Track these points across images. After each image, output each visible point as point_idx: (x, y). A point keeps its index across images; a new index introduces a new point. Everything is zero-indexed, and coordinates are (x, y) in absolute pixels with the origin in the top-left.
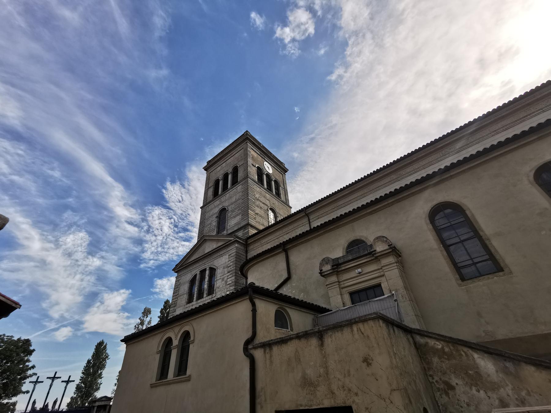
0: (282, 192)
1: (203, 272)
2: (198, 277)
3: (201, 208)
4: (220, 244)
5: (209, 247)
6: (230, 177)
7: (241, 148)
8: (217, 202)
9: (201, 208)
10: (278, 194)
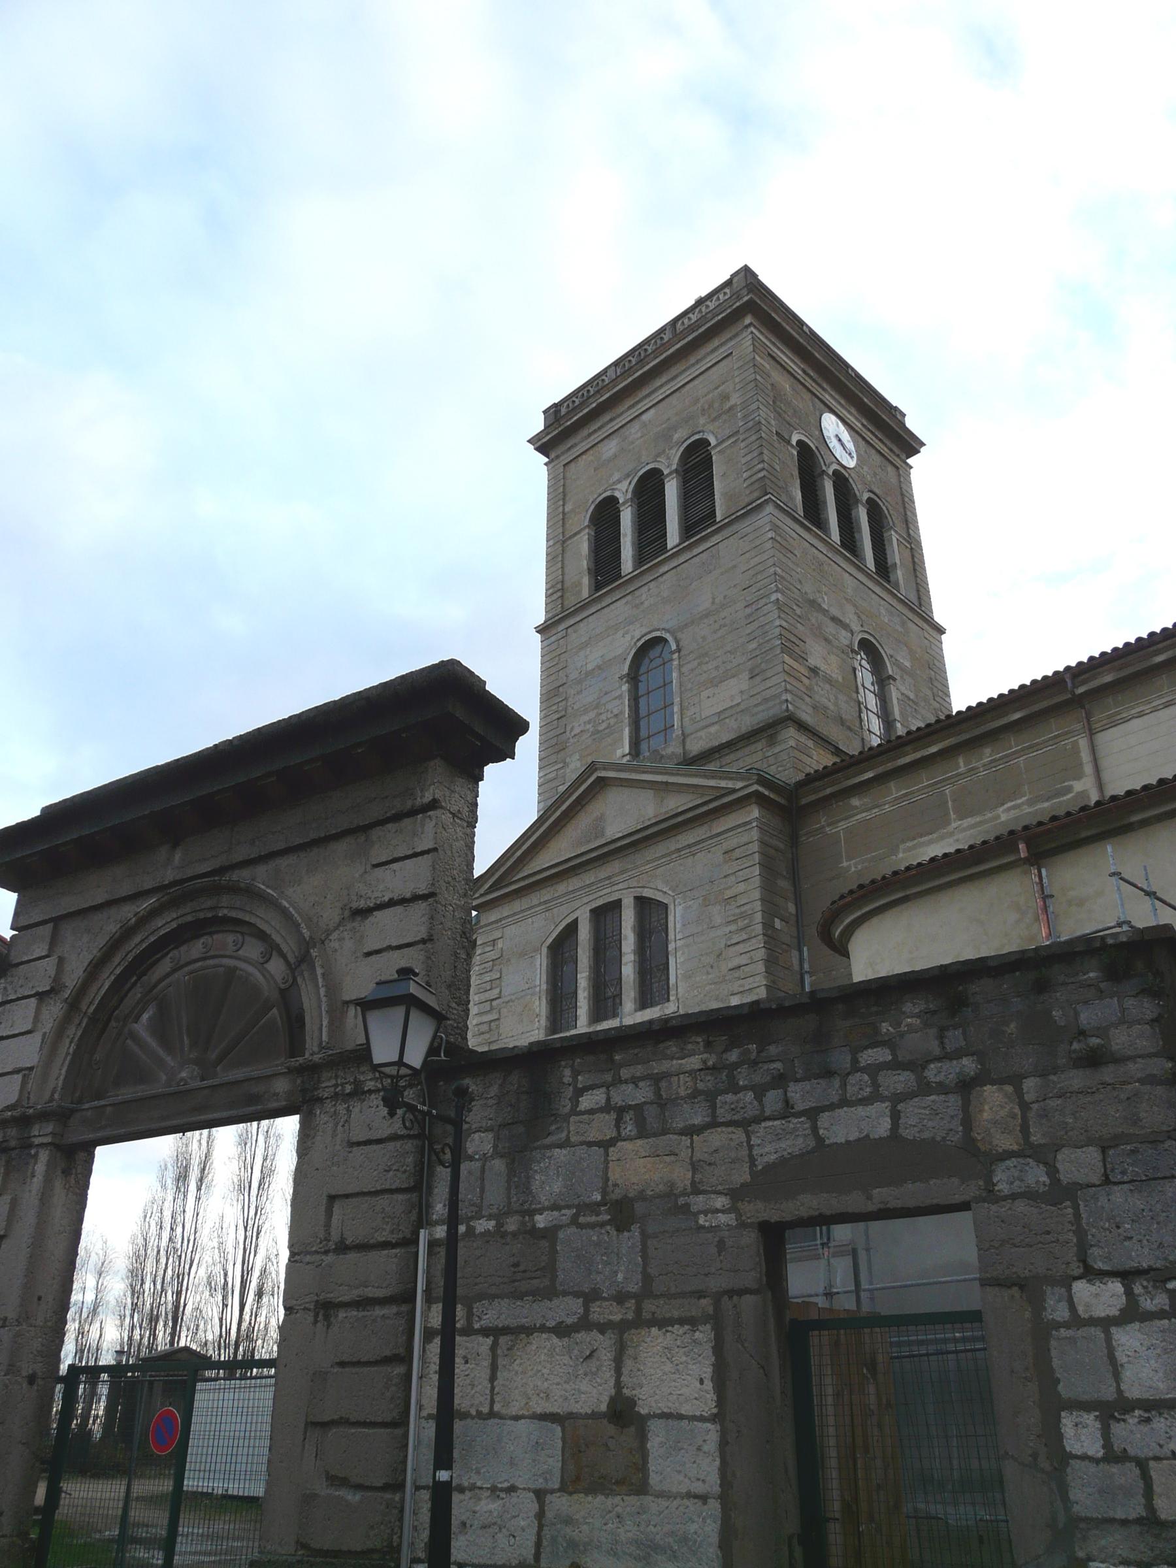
0: (896, 554)
1: (605, 914)
2: (584, 933)
3: (541, 630)
4: (676, 803)
5: (621, 814)
6: (672, 491)
7: (723, 352)
8: (619, 610)
9: (541, 630)
10: (884, 569)
